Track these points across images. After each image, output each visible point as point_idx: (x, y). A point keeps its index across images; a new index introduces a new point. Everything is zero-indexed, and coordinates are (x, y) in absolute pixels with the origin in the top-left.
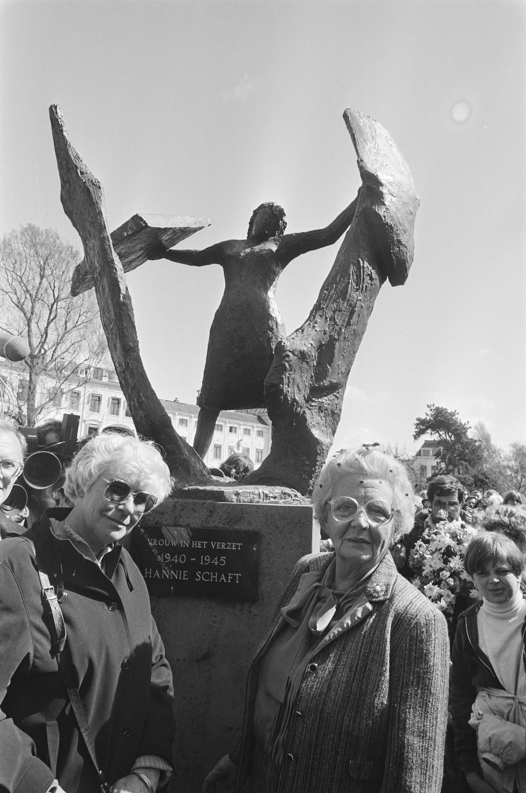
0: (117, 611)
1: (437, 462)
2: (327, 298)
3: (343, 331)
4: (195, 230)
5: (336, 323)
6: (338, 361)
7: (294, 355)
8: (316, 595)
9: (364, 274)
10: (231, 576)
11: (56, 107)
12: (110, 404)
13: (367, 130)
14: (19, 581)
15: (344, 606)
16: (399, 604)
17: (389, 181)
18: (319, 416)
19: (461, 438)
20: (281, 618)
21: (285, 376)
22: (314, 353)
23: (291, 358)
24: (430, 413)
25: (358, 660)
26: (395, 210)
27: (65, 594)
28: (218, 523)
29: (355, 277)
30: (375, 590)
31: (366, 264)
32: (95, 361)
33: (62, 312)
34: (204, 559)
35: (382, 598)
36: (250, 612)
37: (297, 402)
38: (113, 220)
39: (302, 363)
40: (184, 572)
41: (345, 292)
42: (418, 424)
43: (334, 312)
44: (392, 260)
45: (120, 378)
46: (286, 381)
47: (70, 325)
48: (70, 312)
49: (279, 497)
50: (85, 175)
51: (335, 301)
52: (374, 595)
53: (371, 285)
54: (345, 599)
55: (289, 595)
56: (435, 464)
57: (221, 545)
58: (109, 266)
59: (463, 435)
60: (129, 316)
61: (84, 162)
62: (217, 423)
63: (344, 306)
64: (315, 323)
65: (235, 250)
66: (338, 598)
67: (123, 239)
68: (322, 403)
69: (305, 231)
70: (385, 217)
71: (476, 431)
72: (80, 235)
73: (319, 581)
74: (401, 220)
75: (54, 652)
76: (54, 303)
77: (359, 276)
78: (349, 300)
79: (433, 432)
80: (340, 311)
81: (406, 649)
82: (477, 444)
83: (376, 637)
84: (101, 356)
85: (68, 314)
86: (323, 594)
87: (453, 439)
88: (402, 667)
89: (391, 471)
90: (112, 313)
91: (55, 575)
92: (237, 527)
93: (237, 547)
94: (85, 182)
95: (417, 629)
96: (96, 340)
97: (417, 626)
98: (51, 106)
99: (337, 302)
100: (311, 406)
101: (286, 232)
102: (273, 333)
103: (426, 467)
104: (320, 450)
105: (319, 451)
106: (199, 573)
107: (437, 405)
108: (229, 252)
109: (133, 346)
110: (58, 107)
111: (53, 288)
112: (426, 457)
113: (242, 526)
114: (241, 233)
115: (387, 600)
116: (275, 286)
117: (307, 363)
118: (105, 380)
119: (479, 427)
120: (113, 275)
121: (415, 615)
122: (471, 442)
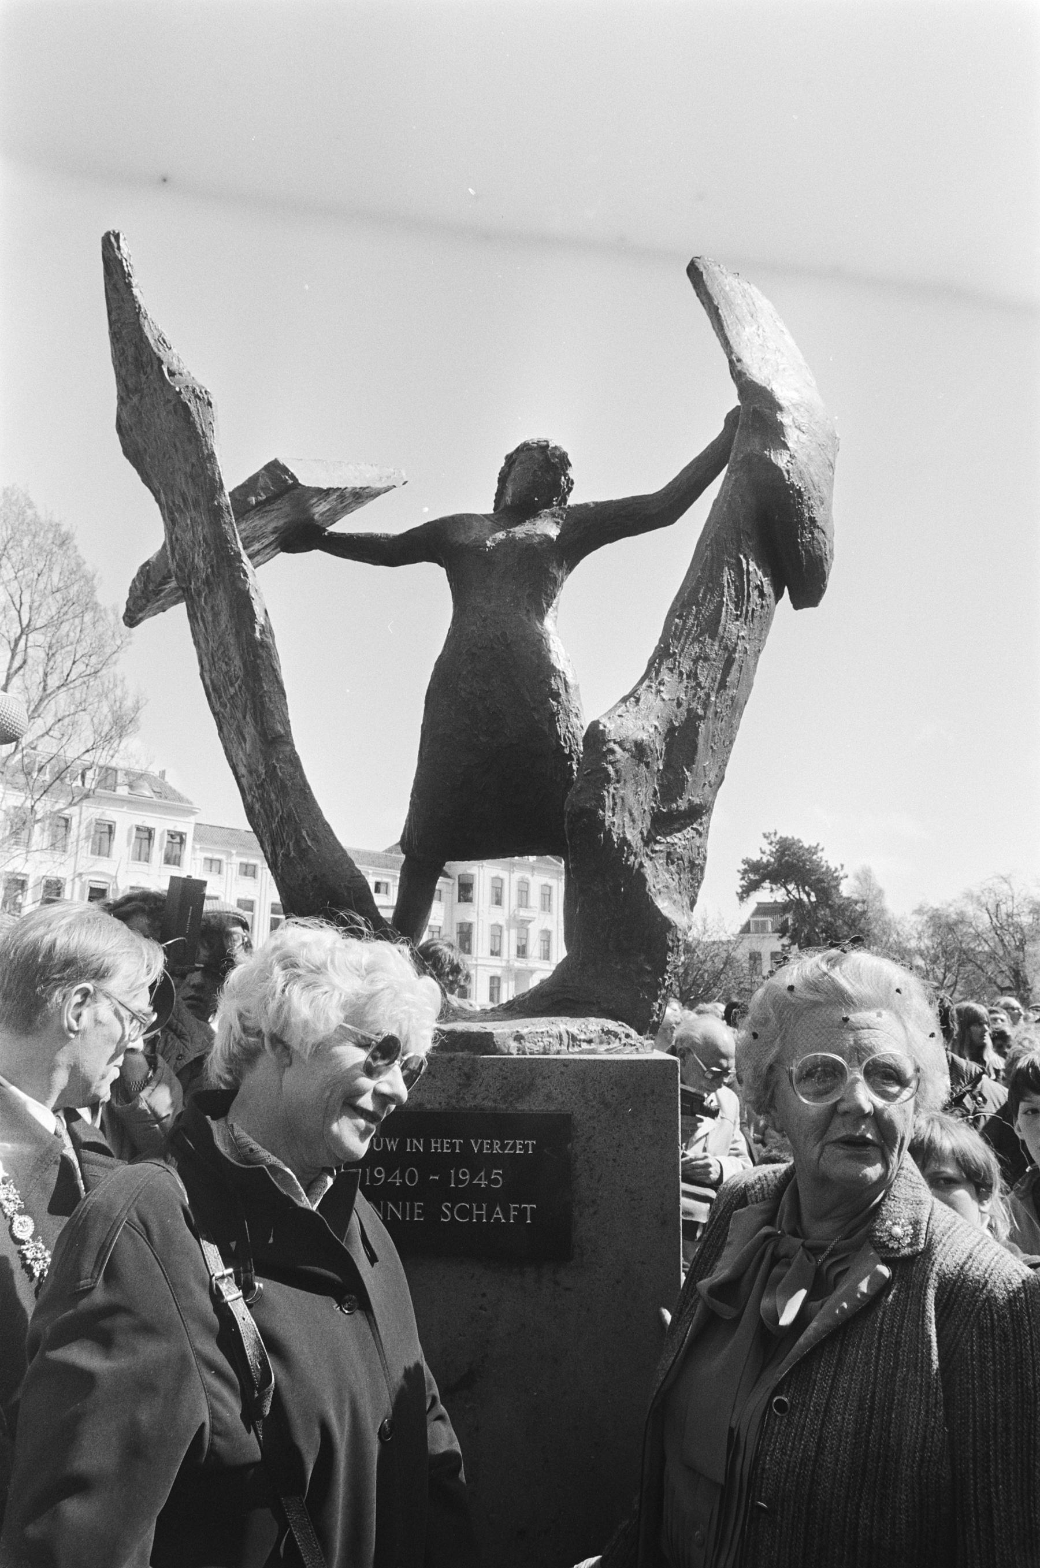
0: (358, 1314)
1: (783, 946)
2: (681, 633)
3: (713, 699)
4: (375, 494)
5: (699, 684)
6: (704, 760)
7: (624, 750)
8: (769, 1251)
9: (749, 586)
10: (515, 1209)
11: (117, 237)
12: (133, 840)
13: (739, 300)
14: (164, 1263)
15: (829, 1269)
16: (947, 1259)
17: (794, 401)
18: (668, 871)
19: (828, 899)
20: (700, 1305)
21: (608, 792)
22: (660, 745)
23: (618, 756)
24: (768, 848)
25: (874, 1384)
26: (805, 459)
27: (258, 1285)
28: (484, 1099)
29: (733, 592)
30: (890, 1235)
31: (753, 566)
32: (105, 753)
33: (37, 655)
34: (456, 1174)
35: (906, 1251)
36: (557, 1283)
37: (630, 846)
38: (235, 467)
39: (638, 766)
40: (416, 1204)
41: (714, 621)
42: (745, 872)
43: (695, 662)
44: (799, 557)
45: (249, 798)
46: (609, 802)
47: (53, 681)
48: (53, 655)
49: (598, 1040)
50: (177, 376)
51: (696, 639)
52: (890, 1246)
53: (762, 607)
54: (830, 1256)
55: (710, 1256)
56: (779, 949)
57: (491, 1145)
58: (230, 566)
59: (833, 891)
60: (274, 670)
61: (174, 350)
62: (437, 887)
63: (713, 649)
64: (660, 684)
65: (473, 535)
66: (814, 1255)
67: (249, 511)
68: (673, 845)
69: (614, 498)
70: (788, 472)
71: (857, 883)
72: (158, 500)
73: (770, 1221)
74: (816, 478)
75: (250, 1414)
76: (20, 637)
77: (739, 590)
78: (723, 637)
79: (774, 887)
80: (706, 659)
81: (972, 1355)
82: (859, 908)
83: (906, 1334)
84: (117, 741)
85: (49, 660)
86: (782, 1251)
87: (813, 899)
88: (968, 1394)
89: (898, 991)
90: (237, 662)
91: (233, 1245)
92: (523, 1107)
93: (525, 1147)
94: (180, 392)
95: (991, 1311)
96: (105, 710)
97: (990, 1306)
98: (108, 234)
99: (700, 641)
100: (654, 851)
101: (573, 500)
102: (559, 703)
103: (760, 954)
104: (673, 941)
105: (670, 944)
106: (447, 1207)
107: (783, 833)
108: (462, 538)
109: (283, 732)
110: (122, 237)
111: (18, 607)
112: (762, 935)
113: (533, 1105)
114: (485, 506)
115: (919, 1253)
116: (556, 608)
117: (647, 765)
118: (123, 791)
119: (862, 877)
120: (240, 585)
121: (983, 1281)
122: (849, 905)
